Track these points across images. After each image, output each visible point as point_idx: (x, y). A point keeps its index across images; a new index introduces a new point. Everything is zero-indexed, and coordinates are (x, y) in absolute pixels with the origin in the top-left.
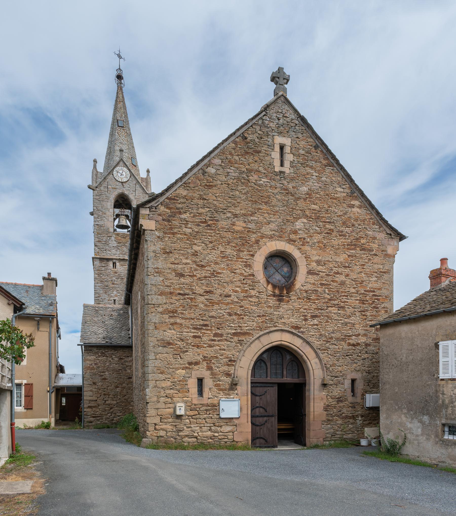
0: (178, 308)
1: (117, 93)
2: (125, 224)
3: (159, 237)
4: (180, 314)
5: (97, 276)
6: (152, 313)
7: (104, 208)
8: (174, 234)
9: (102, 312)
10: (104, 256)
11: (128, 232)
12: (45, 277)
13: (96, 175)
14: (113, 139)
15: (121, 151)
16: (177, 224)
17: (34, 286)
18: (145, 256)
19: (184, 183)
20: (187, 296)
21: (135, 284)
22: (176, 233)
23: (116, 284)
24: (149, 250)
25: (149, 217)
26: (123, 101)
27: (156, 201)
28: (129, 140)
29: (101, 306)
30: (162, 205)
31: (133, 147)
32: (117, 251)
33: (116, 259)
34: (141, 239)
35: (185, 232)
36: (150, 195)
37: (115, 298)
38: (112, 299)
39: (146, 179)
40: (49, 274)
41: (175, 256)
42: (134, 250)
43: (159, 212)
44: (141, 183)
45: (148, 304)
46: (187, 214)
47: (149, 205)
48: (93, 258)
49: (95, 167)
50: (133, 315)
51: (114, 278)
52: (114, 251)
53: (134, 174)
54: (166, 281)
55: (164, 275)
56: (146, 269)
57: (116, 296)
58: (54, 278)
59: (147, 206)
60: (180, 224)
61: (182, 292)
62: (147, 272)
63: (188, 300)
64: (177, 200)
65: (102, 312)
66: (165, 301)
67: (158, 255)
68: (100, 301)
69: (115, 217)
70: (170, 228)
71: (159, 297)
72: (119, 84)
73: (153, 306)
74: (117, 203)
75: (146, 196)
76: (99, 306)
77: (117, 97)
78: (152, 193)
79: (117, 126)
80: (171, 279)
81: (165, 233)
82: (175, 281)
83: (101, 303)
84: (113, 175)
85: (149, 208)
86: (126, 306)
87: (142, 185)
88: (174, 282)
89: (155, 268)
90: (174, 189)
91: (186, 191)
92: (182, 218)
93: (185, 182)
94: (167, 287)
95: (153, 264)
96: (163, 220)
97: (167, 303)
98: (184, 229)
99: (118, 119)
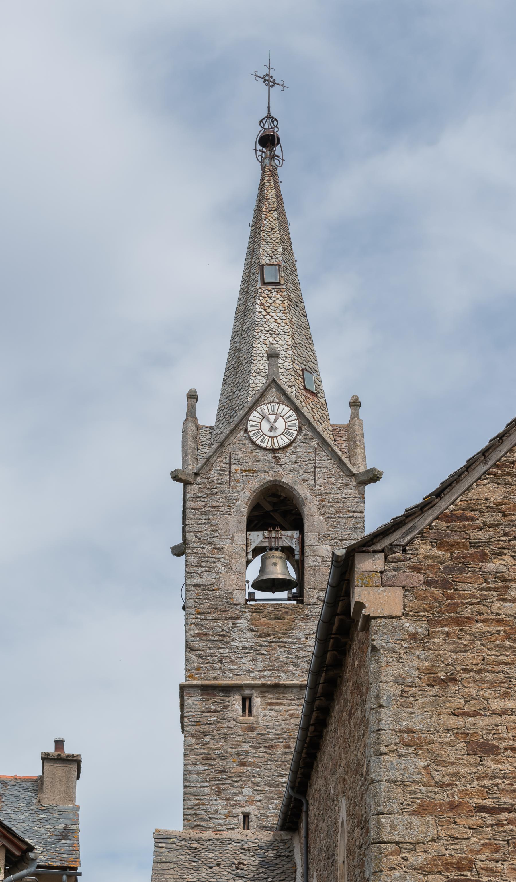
0: (478, 852)
1: (262, 187)
2: (280, 576)
3: (413, 636)
4: (484, 872)
5: (192, 741)
6: (392, 869)
7: (217, 534)
8: (461, 622)
9: (212, 855)
10: (215, 678)
11: (289, 599)
12: (48, 754)
13: (196, 437)
14: (248, 324)
15: (272, 356)
16: (473, 592)
17: (17, 781)
18: (372, 694)
19: (495, 465)
20: (506, 815)
21: (320, 769)
22: (470, 619)
23: (251, 765)
24: (383, 678)
25: (384, 578)
26: (280, 209)
27: (404, 530)
28: (295, 319)
29: (206, 835)
30: (423, 538)
31: (309, 338)
32: (255, 660)
33: (253, 687)
34: (352, 640)
35: (498, 614)
36: (362, 478)
37: (247, 809)
38: (238, 810)
39: (349, 428)
40: (59, 744)
41: (466, 690)
42: (326, 671)
43: (415, 559)
44: (332, 444)
45: (380, 843)
46: (506, 557)
47: (385, 543)
48: (182, 688)
49: (191, 413)
50: (313, 866)
51: (246, 746)
52: (245, 662)
53: (312, 420)
54: (438, 768)
55: (431, 752)
56: (373, 736)
57: (251, 802)
58: (73, 756)
59: (378, 547)
60: (482, 589)
61: (489, 802)
62: (378, 742)
63: (510, 827)
64: (473, 519)
65: (212, 855)
66: (432, 832)
67: (412, 691)
68: (202, 819)
69: (250, 556)
70: (449, 605)
71: (415, 820)
72: (267, 161)
73: (394, 847)
74: (256, 513)
75: (348, 484)
76: (201, 835)
77: (261, 198)
78: (368, 471)
79: (259, 285)
80: (452, 763)
81: (435, 623)
82: (468, 770)
83: (205, 824)
84: (246, 431)
85: (383, 551)
86: (285, 835)
87: (337, 450)
88: (464, 770)
89: (400, 731)
90: (464, 486)
91: (502, 490)
92: (489, 573)
93: (499, 460)
94: (441, 786)
95: (395, 717)
96: (428, 583)
97: (439, 838)
98: (496, 606)
99: (263, 262)
